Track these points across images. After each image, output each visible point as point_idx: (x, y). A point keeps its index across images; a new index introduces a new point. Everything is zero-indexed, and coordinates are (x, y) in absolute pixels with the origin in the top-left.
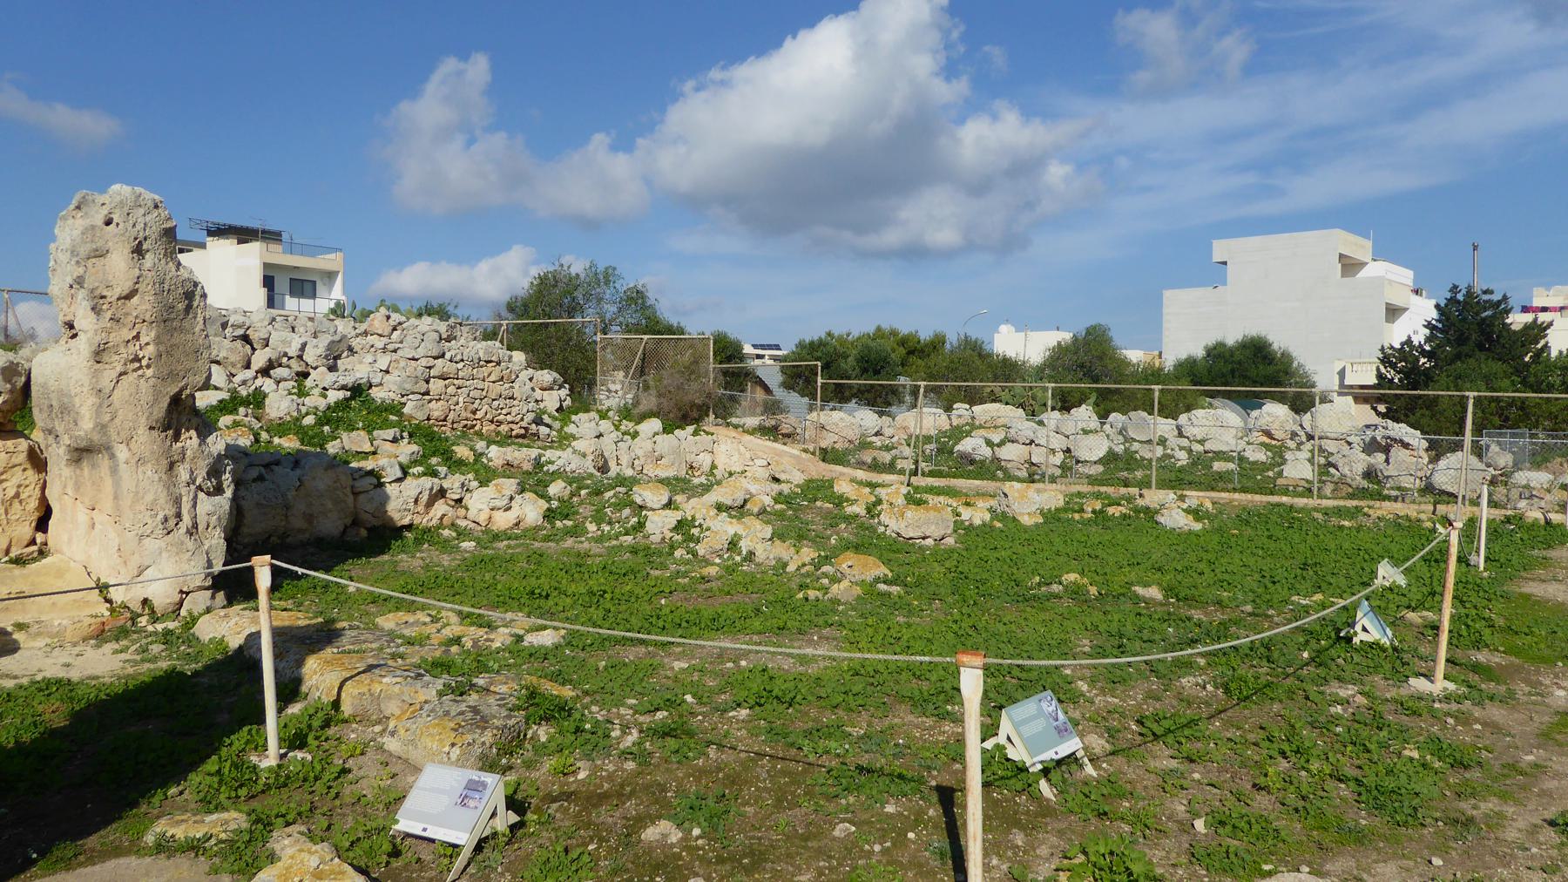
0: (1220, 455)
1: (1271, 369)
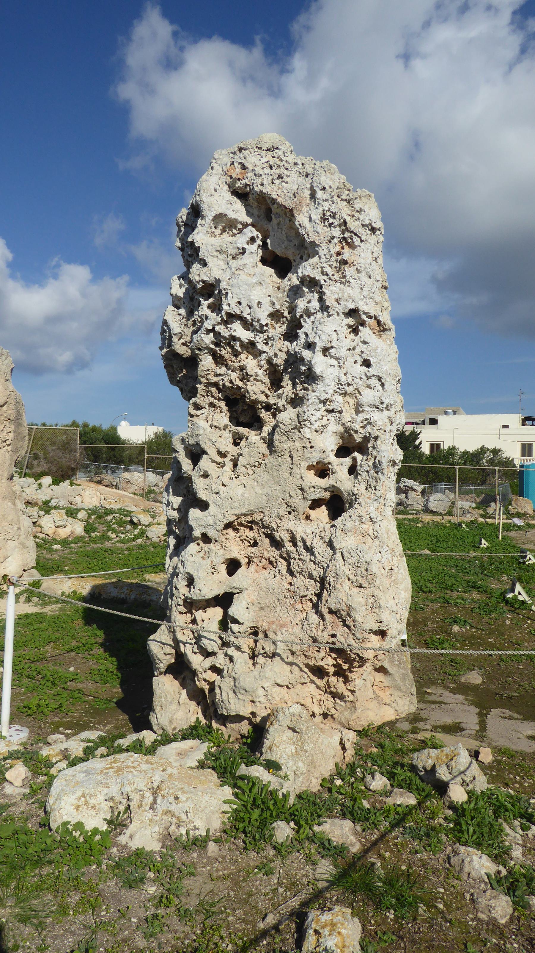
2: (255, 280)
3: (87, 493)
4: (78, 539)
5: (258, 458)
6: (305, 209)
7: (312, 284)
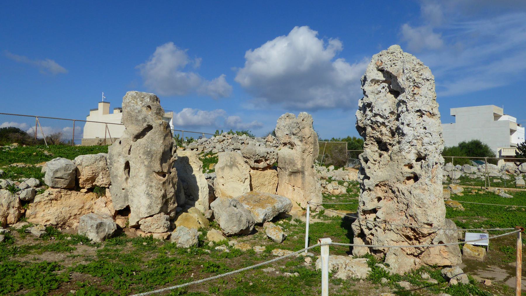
0: (494, 178)
1: (482, 151)
2: (383, 102)
3: (351, 174)
4: (344, 195)
5: (386, 162)
6: (401, 76)
7: (404, 102)
